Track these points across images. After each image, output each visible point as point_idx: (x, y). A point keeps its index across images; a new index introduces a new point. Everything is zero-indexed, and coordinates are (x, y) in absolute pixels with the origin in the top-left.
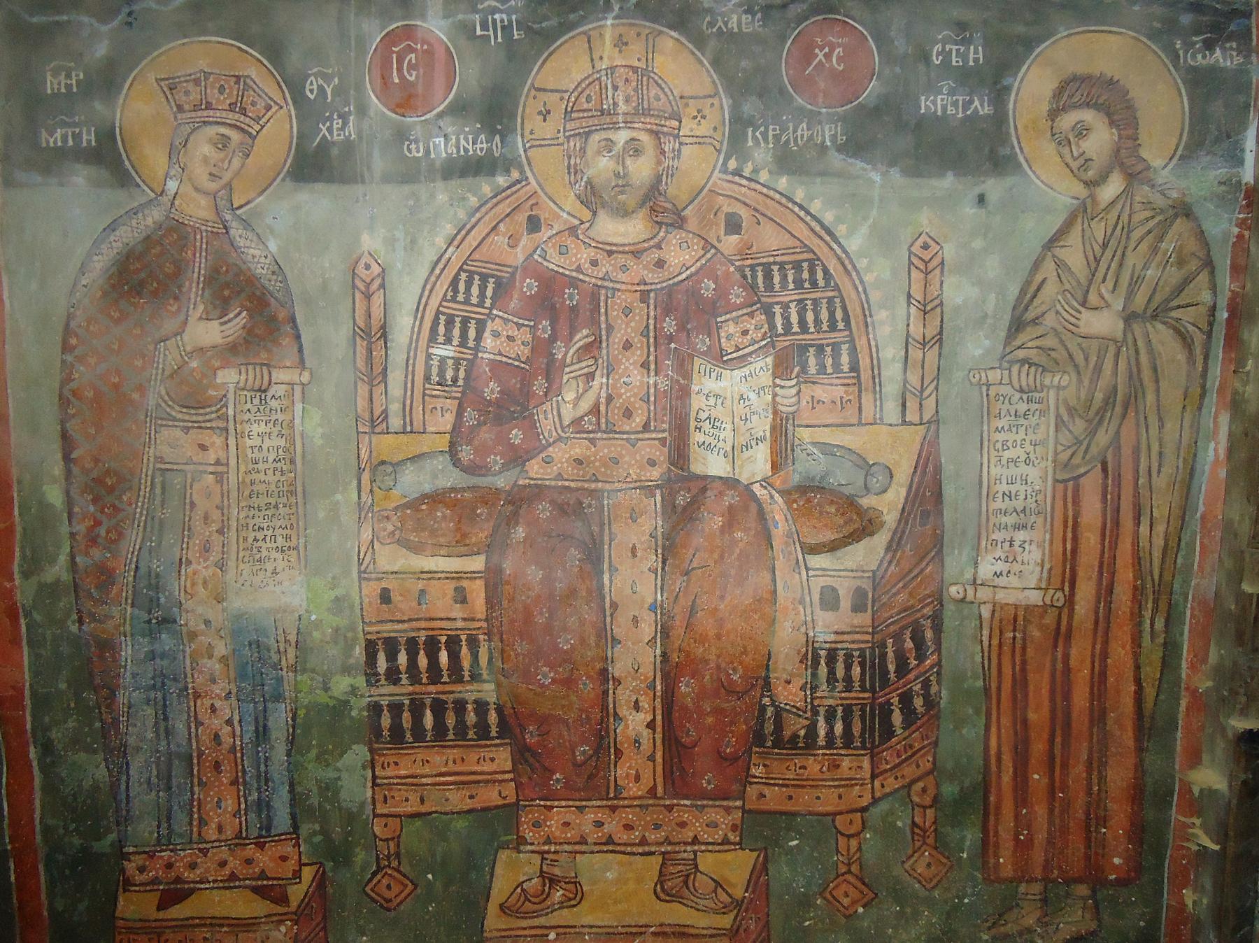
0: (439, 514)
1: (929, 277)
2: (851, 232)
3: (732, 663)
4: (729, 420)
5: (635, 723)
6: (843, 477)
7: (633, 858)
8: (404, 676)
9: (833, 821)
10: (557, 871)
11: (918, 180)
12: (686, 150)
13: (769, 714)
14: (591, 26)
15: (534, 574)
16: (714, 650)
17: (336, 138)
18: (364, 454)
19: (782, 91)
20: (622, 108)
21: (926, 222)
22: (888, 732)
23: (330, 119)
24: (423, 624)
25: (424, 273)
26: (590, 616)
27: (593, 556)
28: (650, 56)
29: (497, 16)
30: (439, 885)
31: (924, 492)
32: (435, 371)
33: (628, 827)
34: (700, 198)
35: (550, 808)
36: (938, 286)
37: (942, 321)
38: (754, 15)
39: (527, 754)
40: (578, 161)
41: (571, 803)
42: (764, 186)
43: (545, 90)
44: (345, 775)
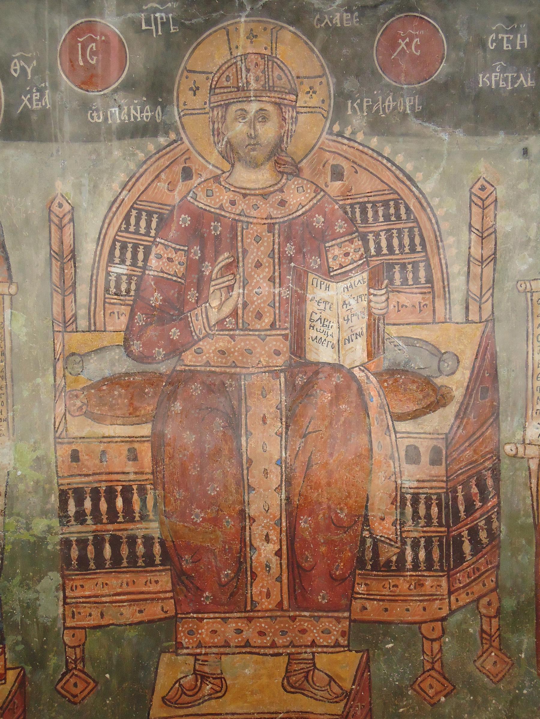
0: (116, 393)
1: (486, 211)
2: (427, 177)
3: (340, 504)
4: (335, 320)
5: (266, 552)
6: (421, 362)
7: (265, 658)
8: (89, 518)
9: (420, 628)
10: (206, 669)
11: (477, 138)
12: (301, 118)
13: (368, 544)
14: (229, 22)
15: (189, 438)
16: (325, 494)
17: (35, 107)
18: (59, 348)
19: (374, 72)
20: (253, 85)
21: (483, 170)
22: (460, 558)
23: (30, 92)
24: (104, 477)
25: (103, 210)
26: (232, 470)
27: (233, 423)
28: (274, 45)
29: (158, 15)
30: (115, 682)
31: (484, 374)
32: (113, 284)
33: (262, 634)
34: (312, 153)
35: (203, 619)
36: (492, 218)
37: (496, 245)
38: (352, 13)
39: (184, 578)
40: (220, 126)
41: (217, 615)
42: (360, 144)
43: (194, 72)
44: (42, 596)
